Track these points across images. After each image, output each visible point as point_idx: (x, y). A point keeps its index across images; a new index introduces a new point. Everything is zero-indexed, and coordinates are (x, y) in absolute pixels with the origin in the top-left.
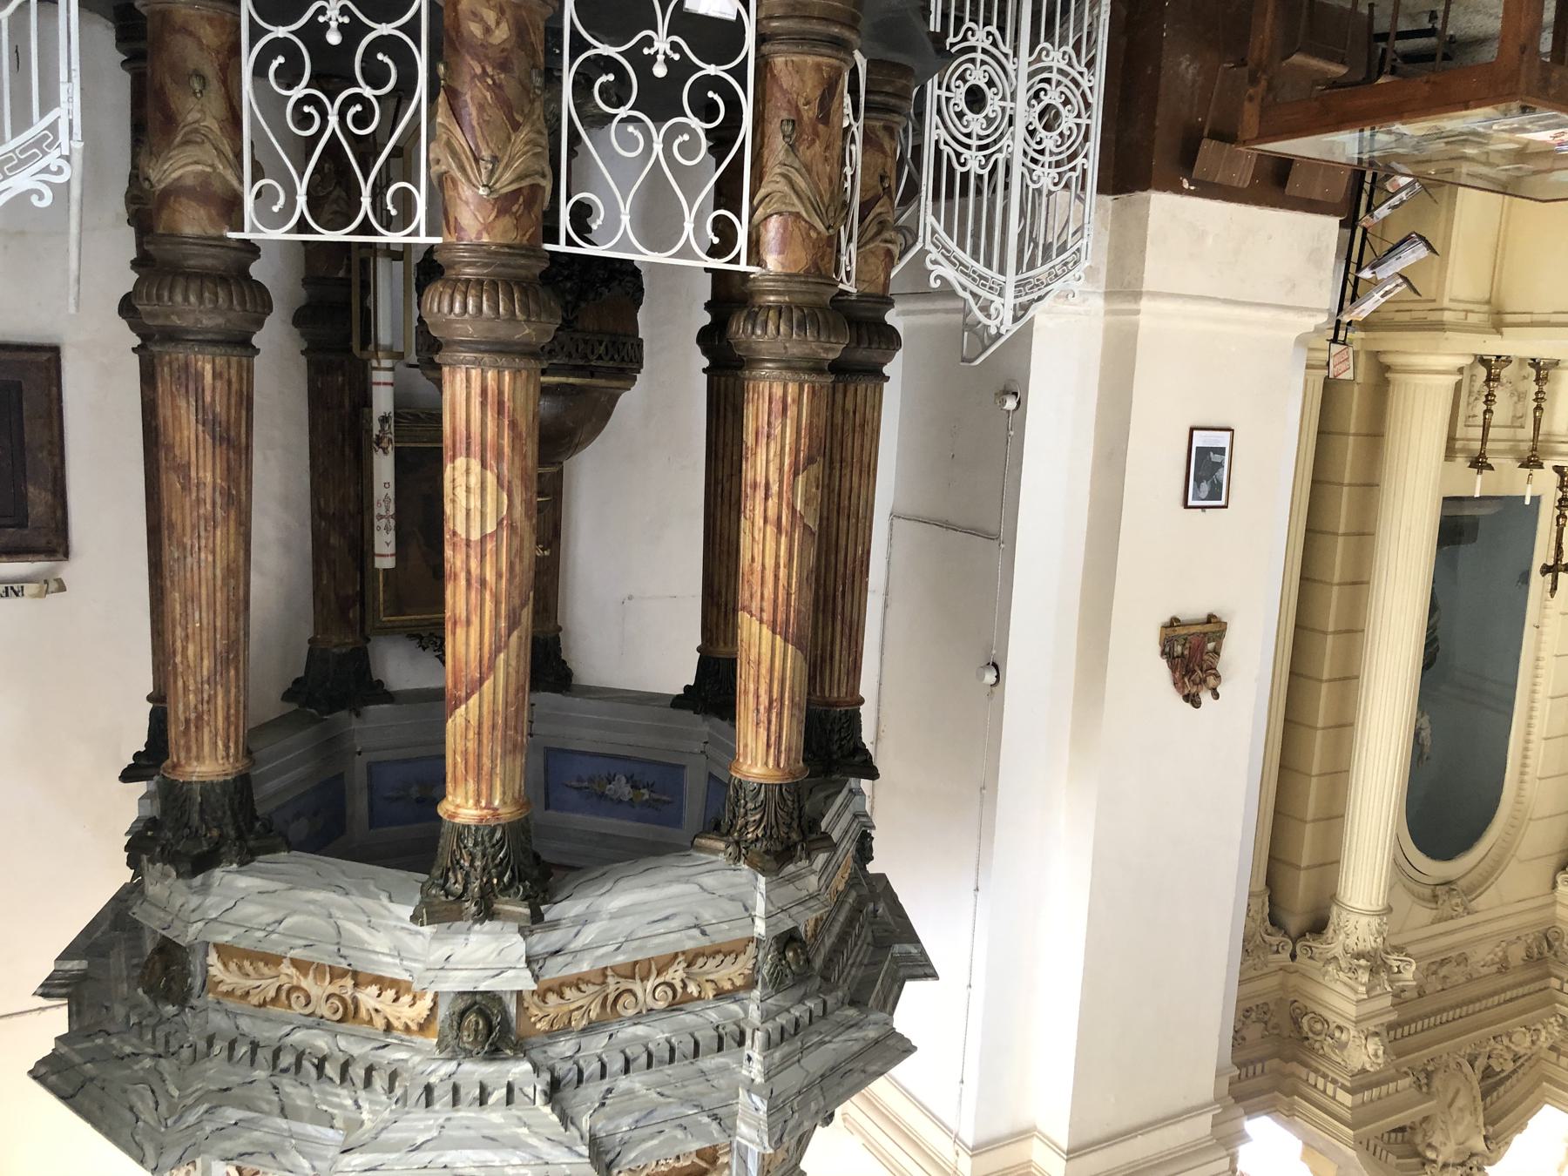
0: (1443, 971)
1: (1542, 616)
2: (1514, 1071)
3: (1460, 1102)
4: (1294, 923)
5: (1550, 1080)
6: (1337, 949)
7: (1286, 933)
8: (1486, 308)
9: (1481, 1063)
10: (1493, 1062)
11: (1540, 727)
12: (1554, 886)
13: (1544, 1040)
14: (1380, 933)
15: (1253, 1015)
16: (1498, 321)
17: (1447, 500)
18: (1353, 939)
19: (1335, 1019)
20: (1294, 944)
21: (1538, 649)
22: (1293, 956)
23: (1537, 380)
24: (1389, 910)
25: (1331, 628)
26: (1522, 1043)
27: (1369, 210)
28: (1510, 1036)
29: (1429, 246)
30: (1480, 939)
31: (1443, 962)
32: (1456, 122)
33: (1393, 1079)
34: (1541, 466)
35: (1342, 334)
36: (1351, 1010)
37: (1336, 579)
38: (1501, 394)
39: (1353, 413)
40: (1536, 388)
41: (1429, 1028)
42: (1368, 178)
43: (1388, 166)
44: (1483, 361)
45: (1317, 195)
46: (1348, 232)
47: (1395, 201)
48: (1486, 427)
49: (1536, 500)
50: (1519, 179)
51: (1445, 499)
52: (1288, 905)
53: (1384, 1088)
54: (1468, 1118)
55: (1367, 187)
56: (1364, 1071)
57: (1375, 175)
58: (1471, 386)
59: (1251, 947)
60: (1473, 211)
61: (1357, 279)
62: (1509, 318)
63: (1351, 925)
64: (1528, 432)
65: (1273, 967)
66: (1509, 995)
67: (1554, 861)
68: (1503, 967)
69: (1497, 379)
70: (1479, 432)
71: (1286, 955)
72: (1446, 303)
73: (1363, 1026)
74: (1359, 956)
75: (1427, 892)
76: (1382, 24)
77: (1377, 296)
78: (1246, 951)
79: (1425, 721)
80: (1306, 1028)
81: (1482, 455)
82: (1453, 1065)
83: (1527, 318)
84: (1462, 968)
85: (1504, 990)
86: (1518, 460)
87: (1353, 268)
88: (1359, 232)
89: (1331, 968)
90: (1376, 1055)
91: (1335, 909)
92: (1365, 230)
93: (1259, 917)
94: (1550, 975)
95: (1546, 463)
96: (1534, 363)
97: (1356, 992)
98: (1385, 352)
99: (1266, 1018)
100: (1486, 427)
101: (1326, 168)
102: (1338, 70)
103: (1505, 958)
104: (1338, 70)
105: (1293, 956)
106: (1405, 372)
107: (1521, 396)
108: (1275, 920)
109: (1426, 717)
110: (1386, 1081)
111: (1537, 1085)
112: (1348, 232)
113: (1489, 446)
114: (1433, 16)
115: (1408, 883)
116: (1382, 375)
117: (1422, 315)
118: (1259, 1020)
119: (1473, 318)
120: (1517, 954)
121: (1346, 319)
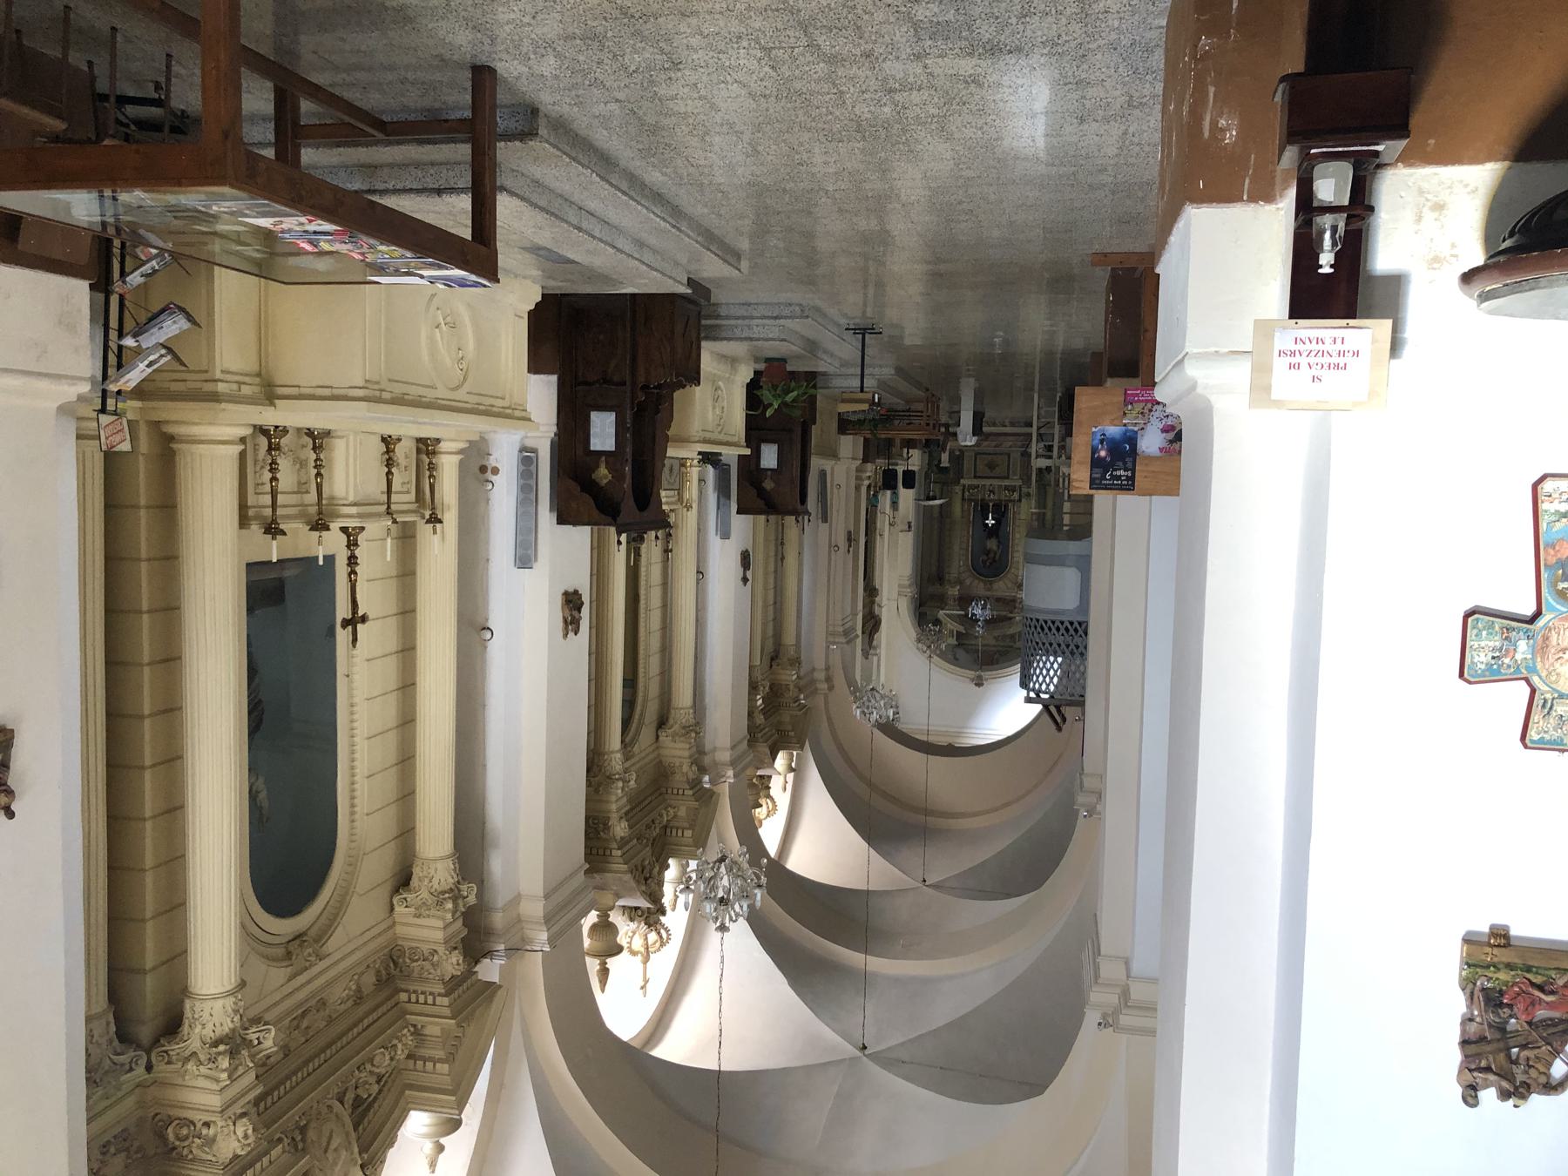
0: (305, 1024)
1: (350, 665)
2: (380, 1091)
3: (334, 1145)
4: (145, 1033)
5: (412, 1087)
6: (194, 1044)
7: (139, 1046)
8: (257, 380)
9: (350, 1097)
10: (360, 1091)
11: (362, 768)
12: (392, 909)
13: (401, 1054)
14: (236, 1011)
15: (112, 1150)
16: (270, 393)
17: (251, 567)
18: (210, 1026)
19: (199, 1117)
20: (148, 1053)
21: (351, 696)
22: (149, 1068)
23: (314, 448)
24: (242, 984)
25: (147, 712)
26: (383, 1062)
27: (123, 274)
28: (371, 1061)
29: (190, 318)
30: (329, 984)
31: (304, 1014)
32: (191, 198)
33: (267, 1153)
34: (328, 529)
35: (110, 402)
36: (215, 1101)
37: (146, 659)
38: (284, 463)
39: (142, 486)
40: (314, 456)
41: (292, 1088)
42: (117, 243)
43: (134, 232)
44: (262, 430)
45: (57, 254)
46: (101, 296)
47: (146, 268)
48: (274, 494)
49: (330, 559)
50: (269, 262)
51: (248, 565)
52: (133, 1011)
53: (258, 1166)
54: (344, 1154)
55: (116, 251)
56: (236, 1157)
57: (123, 245)
58: (256, 455)
59: (95, 1076)
60: (231, 292)
61: (120, 348)
62: (280, 391)
63: (206, 1015)
64: (312, 497)
65: (126, 1088)
66: (366, 1022)
67: (388, 887)
68: (359, 998)
69: (278, 448)
70: (267, 499)
71: (140, 1070)
72: (218, 375)
73: (230, 1112)
74: (216, 1044)
75: (280, 951)
76: (102, 86)
77: (142, 366)
78: (91, 1081)
79: (260, 784)
80: (171, 1137)
81: (274, 521)
82: (325, 1110)
83: (327, 392)
84: (322, 1013)
85: (361, 1020)
86: (307, 523)
87: (113, 335)
88: (114, 300)
89: (190, 1066)
90: (246, 1136)
91: (188, 1004)
92: (122, 297)
93: (104, 1041)
94: (398, 991)
95: (332, 526)
96: (310, 433)
97: (217, 1081)
98: (167, 422)
99: (127, 1144)
100: (274, 494)
101: (69, 231)
102: (60, 126)
103: (359, 990)
104: (60, 126)
105: (149, 1068)
106: (188, 442)
107: (303, 464)
108: (124, 1037)
109: (261, 780)
110: (259, 1158)
111: (402, 1093)
112: (101, 296)
113: (279, 512)
114: (158, 87)
115: (262, 948)
116: (167, 449)
117: (198, 385)
118: (118, 1151)
119: (246, 390)
120: (369, 979)
121: (113, 388)
